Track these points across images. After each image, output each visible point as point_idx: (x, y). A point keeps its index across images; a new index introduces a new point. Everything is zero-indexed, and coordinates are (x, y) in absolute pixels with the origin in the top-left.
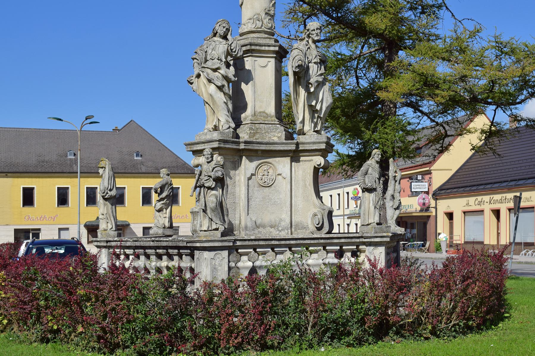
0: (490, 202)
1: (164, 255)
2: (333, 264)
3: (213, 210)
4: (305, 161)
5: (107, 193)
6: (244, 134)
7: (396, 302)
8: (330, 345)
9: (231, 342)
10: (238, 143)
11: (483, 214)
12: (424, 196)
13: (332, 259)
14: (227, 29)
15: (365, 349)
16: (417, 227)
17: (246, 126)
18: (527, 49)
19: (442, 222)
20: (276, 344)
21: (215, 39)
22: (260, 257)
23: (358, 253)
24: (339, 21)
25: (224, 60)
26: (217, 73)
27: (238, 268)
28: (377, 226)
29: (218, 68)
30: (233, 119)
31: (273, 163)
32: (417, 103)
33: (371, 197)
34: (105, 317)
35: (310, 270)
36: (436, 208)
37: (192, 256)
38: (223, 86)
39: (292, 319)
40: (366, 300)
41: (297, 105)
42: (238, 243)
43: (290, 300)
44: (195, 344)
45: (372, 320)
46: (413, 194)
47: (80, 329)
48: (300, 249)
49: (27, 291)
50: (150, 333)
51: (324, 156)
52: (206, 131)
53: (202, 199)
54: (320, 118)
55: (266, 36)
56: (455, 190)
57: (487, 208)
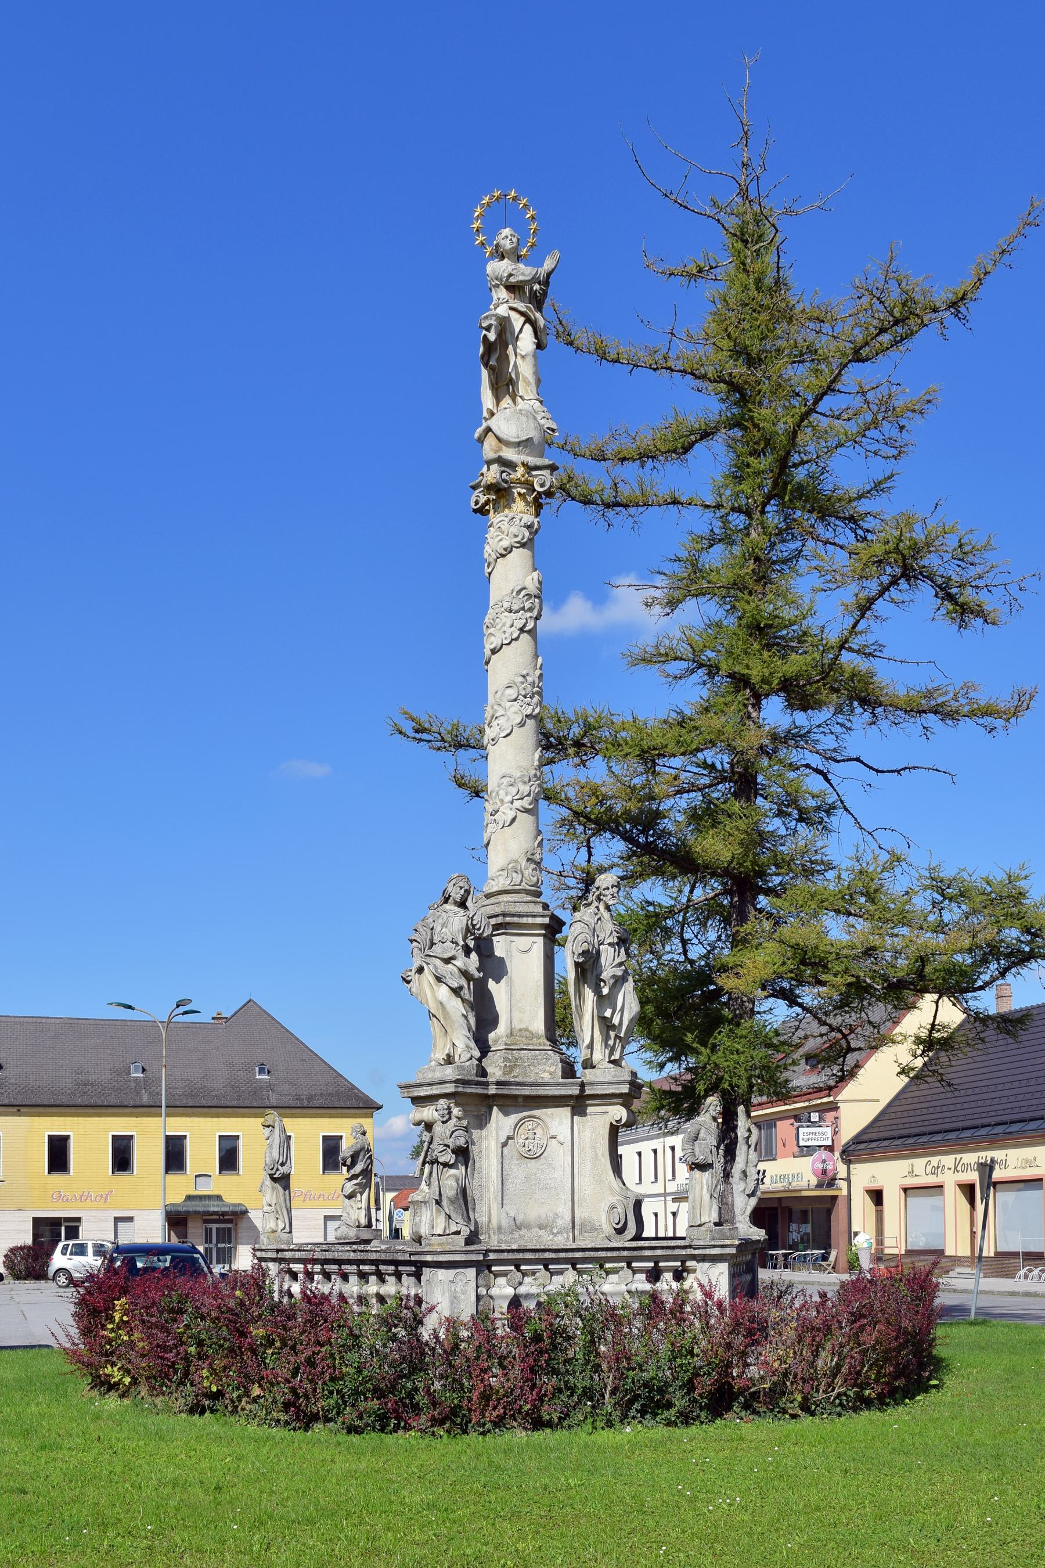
0: (955, 1168)
1: (372, 1274)
2: (643, 1292)
3: (452, 1201)
4: (596, 1113)
5: (278, 1170)
6: (495, 1070)
7: (744, 1355)
8: (640, 1422)
9: (487, 1415)
10: (486, 1084)
11: (942, 1194)
12: (825, 1154)
13: (641, 1284)
14: (466, 891)
15: (694, 1430)
16: (795, 1223)
17: (498, 1053)
18: (989, 889)
19: (861, 1208)
20: (556, 1420)
21: (447, 907)
22: (527, 1280)
23: (685, 1274)
24: (649, 849)
25: (462, 943)
26: (450, 966)
27: (491, 1297)
28: (714, 1228)
29: (453, 958)
30: (477, 1041)
31: (543, 1117)
32: (791, 991)
33: (705, 1178)
34: (295, 1372)
35: (608, 1301)
36: (848, 1180)
37: (418, 1276)
38: (461, 988)
39: (580, 1382)
40: (695, 1351)
41: (581, 1017)
42: (492, 1256)
43: (575, 1351)
44: (433, 1416)
45: (706, 1384)
46: (802, 1151)
47: (256, 1391)
48: (590, 1266)
49: (168, 1331)
50: (366, 1399)
51: (627, 1105)
52: (433, 1063)
53: (435, 1184)
54: (620, 1038)
55: (529, 898)
56: (886, 1143)
57: (950, 1180)
